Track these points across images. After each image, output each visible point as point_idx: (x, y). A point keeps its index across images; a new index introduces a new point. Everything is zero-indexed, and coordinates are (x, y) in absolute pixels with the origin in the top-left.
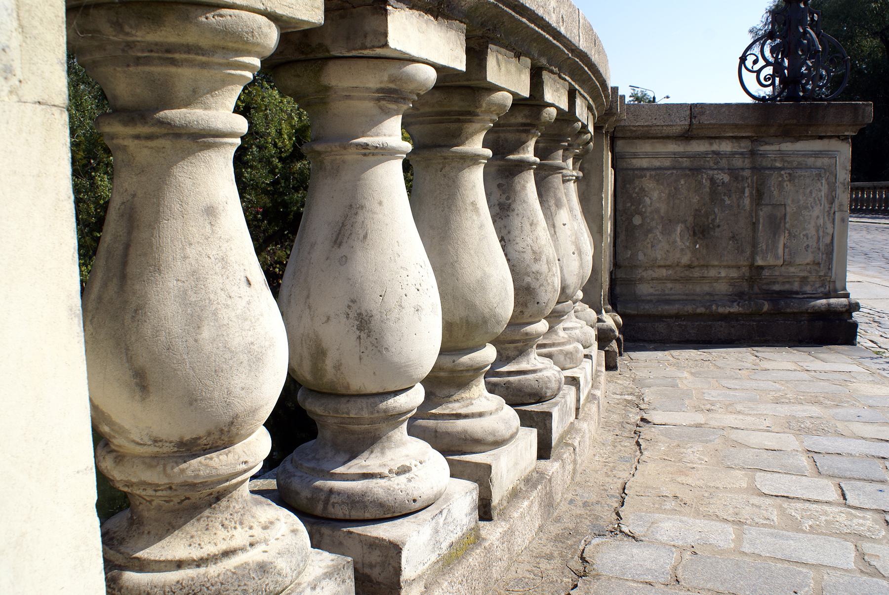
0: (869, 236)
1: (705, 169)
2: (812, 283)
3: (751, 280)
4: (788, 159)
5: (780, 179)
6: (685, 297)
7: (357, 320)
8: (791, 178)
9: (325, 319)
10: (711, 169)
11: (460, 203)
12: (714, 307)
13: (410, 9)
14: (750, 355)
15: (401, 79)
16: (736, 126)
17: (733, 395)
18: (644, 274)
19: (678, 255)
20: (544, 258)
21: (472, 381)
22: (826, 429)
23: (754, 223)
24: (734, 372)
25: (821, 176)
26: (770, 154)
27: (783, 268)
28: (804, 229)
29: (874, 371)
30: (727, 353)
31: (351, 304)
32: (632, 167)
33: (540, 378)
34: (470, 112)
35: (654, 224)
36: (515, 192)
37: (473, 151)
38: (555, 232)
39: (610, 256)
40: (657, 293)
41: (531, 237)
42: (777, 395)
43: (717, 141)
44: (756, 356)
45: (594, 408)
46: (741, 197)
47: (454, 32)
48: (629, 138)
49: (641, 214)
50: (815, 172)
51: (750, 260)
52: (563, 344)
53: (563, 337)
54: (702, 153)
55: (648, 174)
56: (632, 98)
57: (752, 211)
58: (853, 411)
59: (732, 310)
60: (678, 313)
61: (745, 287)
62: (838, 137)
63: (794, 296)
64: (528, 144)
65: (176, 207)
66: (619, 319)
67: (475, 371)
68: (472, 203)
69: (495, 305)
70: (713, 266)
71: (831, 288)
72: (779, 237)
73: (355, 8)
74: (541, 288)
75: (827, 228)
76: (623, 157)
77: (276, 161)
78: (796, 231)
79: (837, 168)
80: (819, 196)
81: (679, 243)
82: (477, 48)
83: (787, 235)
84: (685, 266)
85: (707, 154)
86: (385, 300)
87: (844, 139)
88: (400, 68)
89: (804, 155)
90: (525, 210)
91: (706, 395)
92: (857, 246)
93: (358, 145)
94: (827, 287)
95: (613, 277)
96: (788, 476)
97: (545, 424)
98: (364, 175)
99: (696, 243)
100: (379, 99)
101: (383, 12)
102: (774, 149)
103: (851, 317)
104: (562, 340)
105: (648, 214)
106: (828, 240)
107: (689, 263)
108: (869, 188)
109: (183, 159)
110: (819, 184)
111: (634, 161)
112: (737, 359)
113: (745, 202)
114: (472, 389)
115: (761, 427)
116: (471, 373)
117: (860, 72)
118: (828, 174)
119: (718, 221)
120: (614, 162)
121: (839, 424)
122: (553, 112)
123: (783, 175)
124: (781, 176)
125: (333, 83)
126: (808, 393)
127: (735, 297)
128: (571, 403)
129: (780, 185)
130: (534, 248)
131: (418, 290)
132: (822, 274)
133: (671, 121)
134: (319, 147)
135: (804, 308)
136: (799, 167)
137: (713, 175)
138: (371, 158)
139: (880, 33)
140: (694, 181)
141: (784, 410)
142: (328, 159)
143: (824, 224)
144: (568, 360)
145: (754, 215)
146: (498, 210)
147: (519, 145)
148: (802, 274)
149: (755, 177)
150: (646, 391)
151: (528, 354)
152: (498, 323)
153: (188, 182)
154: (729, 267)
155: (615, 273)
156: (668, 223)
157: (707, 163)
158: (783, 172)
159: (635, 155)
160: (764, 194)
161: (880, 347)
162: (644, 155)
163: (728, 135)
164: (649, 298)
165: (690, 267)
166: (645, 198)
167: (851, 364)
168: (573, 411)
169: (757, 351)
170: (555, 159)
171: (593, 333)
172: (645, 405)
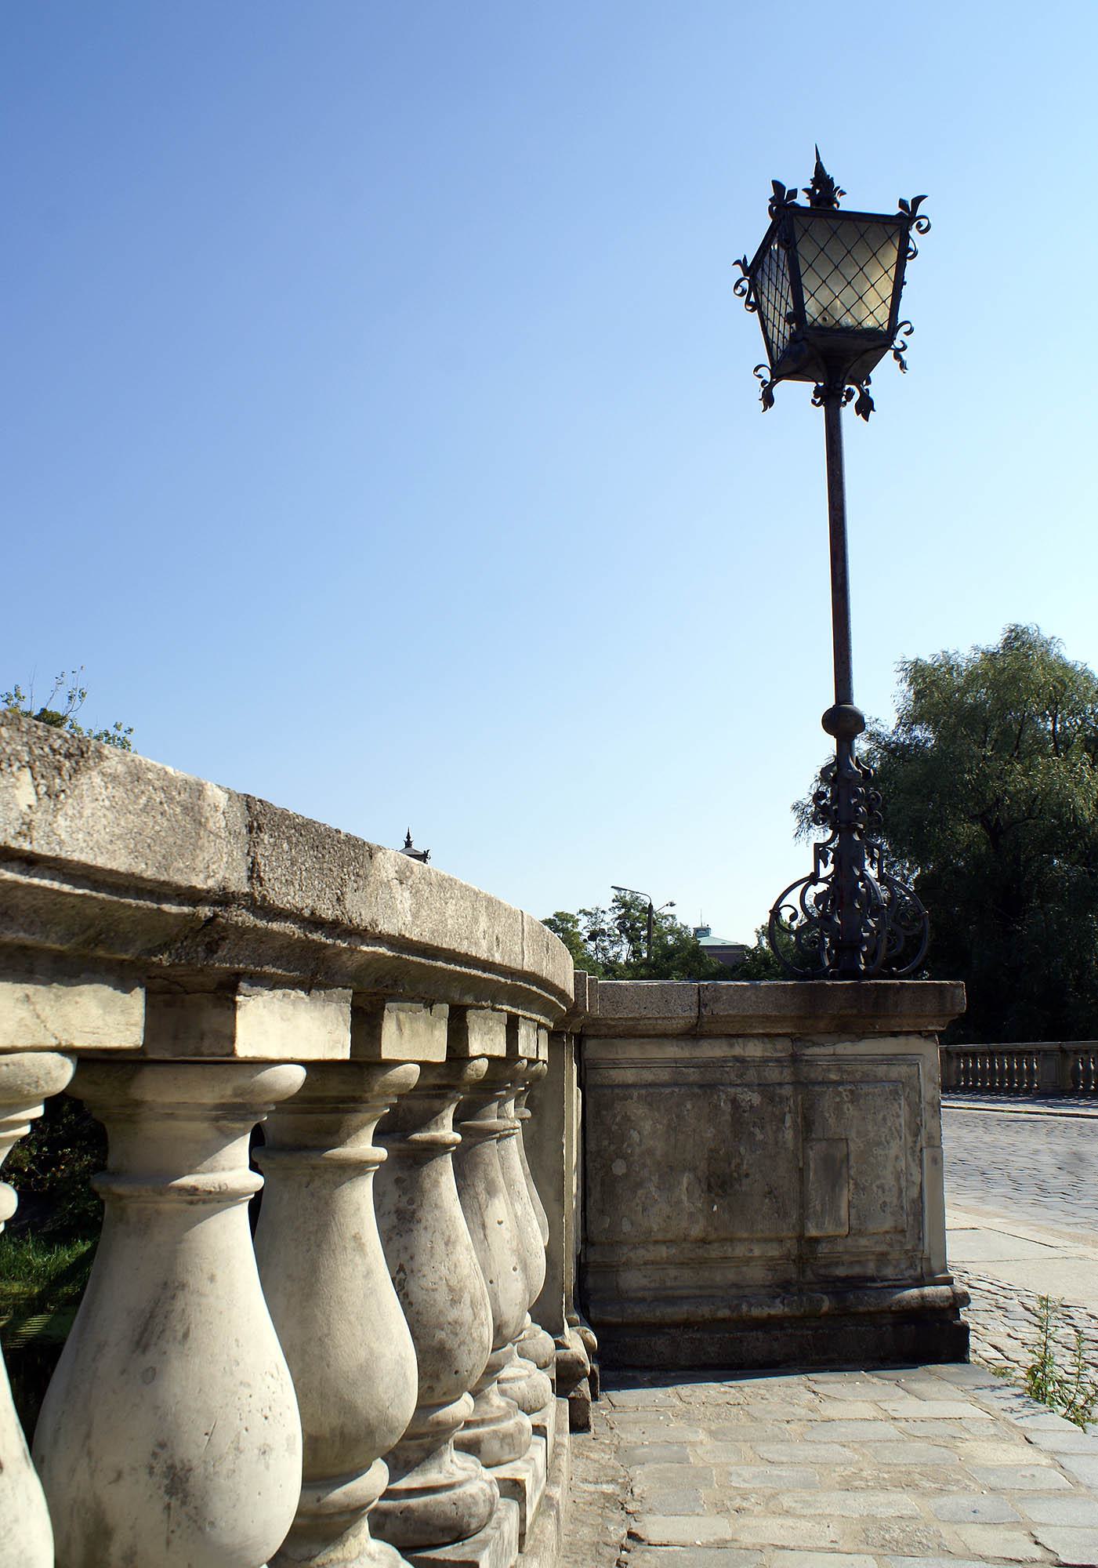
0: (987, 1138)
1: (723, 1085)
2: (894, 1262)
3: (801, 1261)
5: (838, 1099)
6: (698, 1292)
7: (166, 1477)
8: (855, 1098)
9: (113, 1476)
11: (336, 1239)
12: (744, 1308)
13: (271, 990)
14: (805, 1391)
15: (252, 1091)
16: (768, 1018)
17: (778, 1476)
18: (631, 1254)
19: (684, 1224)
20: (467, 1298)
21: (348, 1528)
22: (924, 1541)
23: (801, 1170)
24: (779, 1428)
25: (897, 1093)
26: (820, 1061)
27: (849, 1239)
28: (878, 1177)
29: (996, 1414)
30: (767, 1387)
31: (158, 1450)
32: (610, 1082)
33: (460, 1499)
34: (354, 1097)
35: (645, 1173)
36: (422, 1192)
37: (358, 1157)
38: (485, 1235)
39: (576, 1231)
40: (653, 1285)
41: (446, 1264)
42: (847, 1472)
43: (740, 1040)
44: (814, 1392)
45: (550, 1526)
46: (779, 1129)
47: (334, 1005)
48: (606, 1036)
49: (624, 1157)
50: (889, 1087)
51: (798, 1228)
53: (498, 1407)
54: (718, 1059)
56: (616, 904)
57: (798, 1149)
58: (965, 1501)
59: (773, 1312)
60: (688, 1319)
61: (792, 1272)
62: (920, 1033)
63: (869, 1285)
64: (443, 1114)
66: (593, 1338)
67: (353, 1512)
68: (355, 1237)
69: (387, 1404)
70: (740, 1240)
71: (924, 1270)
72: (841, 1190)
73: (188, 994)
74: (462, 1347)
75: (911, 1175)
78: (866, 1181)
79: (921, 1080)
80: (897, 1125)
82: (368, 1009)
83: (852, 1186)
85: (725, 1061)
87: (928, 1035)
88: (252, 1077)
89: (874, 1062)
90: (437, 1220)
91: (733, 1478)
92: (970, 1158)
93: (182, 1190)
94: (919, 1269)
95: (582, 1261)
98: (189, 1235)
99: (713, 1202)
100: (217, 1119)
101: (232, 1006)
102: (827, 1052)
103: (958, 1317)
104: (497, 1414)
106: (914, 1192)
107: (701, 1235)
108: (983, 1054)
111: (612, 1072)
113: (786, 1136)
114: (348, 1544)
115: (823, 1544)
117: (957, 871)
118: (908, 1090)
119: (745, 1166)
120: (583, 1074)
121: (946, 1531)
122: (483, 1065)
123: (841, 1092)
125: (149, 1096)
126: (895, 1465)
127: (778, 1290)
128: (511, 1532)
129: (838, 1109)
130: (451, 1283)
131: (266, 1418)
132: (909, 1247)
134: (120, 1189)
135: (885, 1304)
136: (866, 1079)
137: (736, 1094)
138: (200, 1207)
139: (981, 816)
141: (858, 1504)
144: (506, 1448)
146: (396, 1221)
147: (429, 1118)
148: (879, 1249)
149: (800, 1097)
150: (638, 1472)
151: (441, 1455)
152: (392, 1431)
154: (766, 1240)
155: (585, 1254)
156: (669, 1171)
157: (726, 1075)
158: (840, 1089)
159: (614, 1063)
160: (814, 1124)
161: (1007, 1358)
163: (755, 1032)
164: (640, 1294)
165: (704, 1241)
167: (963, 1401)
168: (514, 1543)
169: (816, 1382)
170: (485, 1118)
171: (544, 1380)
172: (634, 1503)
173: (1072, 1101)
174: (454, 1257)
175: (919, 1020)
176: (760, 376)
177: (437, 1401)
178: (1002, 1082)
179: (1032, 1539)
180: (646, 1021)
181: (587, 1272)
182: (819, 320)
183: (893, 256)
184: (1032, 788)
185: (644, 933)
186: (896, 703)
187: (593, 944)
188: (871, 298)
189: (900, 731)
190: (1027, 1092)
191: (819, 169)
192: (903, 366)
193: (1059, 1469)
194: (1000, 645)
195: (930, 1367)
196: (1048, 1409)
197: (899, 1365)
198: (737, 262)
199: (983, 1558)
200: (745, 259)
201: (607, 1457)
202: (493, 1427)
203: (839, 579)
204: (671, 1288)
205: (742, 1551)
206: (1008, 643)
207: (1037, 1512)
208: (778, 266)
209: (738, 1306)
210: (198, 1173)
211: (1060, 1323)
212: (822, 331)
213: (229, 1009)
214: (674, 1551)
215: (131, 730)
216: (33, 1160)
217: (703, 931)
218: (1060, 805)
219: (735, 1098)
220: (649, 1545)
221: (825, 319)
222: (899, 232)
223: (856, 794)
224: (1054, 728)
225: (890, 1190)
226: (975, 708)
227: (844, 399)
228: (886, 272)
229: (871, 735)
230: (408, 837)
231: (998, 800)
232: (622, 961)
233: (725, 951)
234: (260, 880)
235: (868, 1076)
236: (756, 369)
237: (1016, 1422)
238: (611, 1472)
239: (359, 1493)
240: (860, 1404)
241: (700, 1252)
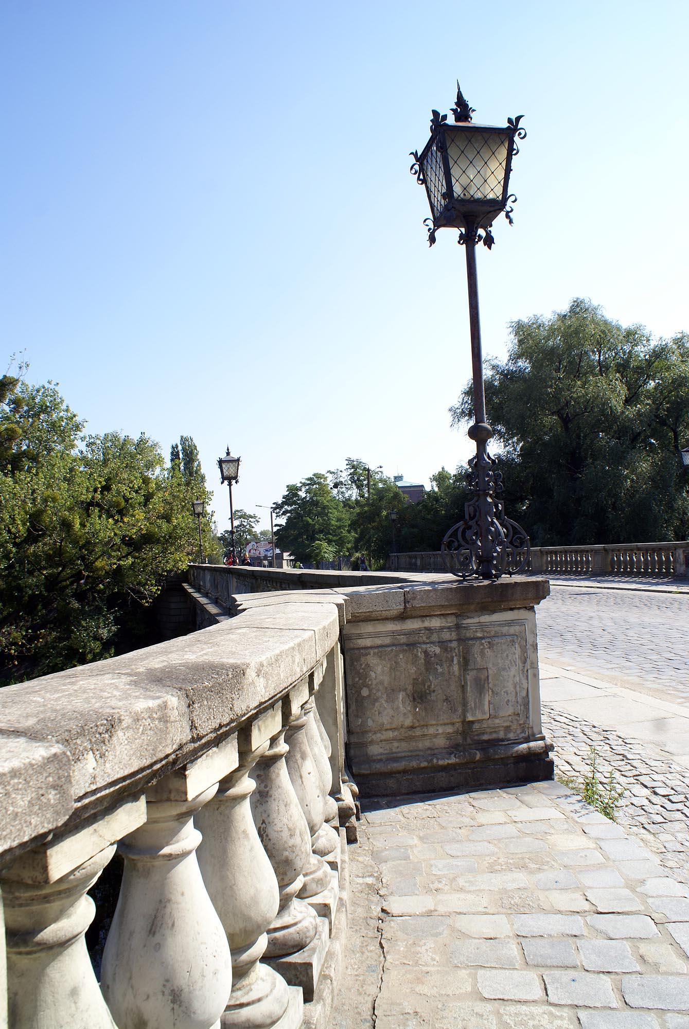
0: (564, 609)
1: (419, 644)
2: (514, 731)
4: (487, 630)
5: (482, 647)
6: (409, 754)
8: (491, 645)
9: (146, 997)
10: (425, 643)
11: (234, 835)
12: (435, 761)
18: (374, 737)
19: (401, 719)
22: (531, 904)
23: (463, 686)
24: (456, 833)
25: (514, 641)
27: (489, 720)
28: (504, 687)
31: (165, 983)
35: (379, 694)
36: (271, 781)
40: (386, 752)
43: (428, 618)
45: (343, 917)
46: (450, 665)
49: (368, 686)
51: (462, 717)
52: (314, 872)
53: (314, 864)
54: (416, 630)
55: (372, 652)
56: (348, 466)
59: (450, 762)
60: (405, 769)
61: (460, 740)
62: (526, 608)
65: (50, 999)
68: (243, 831)
72: (485, 695)
76: (350, 639)
77: (10, 546)
81: (402, 708)
83: (490, 693)
84: (408, 728)
86: (192, 974)
90: (280, 794)
91: (433, 868)
93: (164, 856)
96: (503, 971)
97: (307, 973)
98: (170, 875)
99: (416, 707)
105: (374, 686)
106: (524, 694)
107: (411, 724)
108: (561, 552)
109: (54, 960)
110: (513, 648)
111: (359, 641)
112: (457, 813)
113: (454, 669)
115: (481, 909)
116: (249, 965)
119: (433, 686)
124: (482, 644)
129: (482, 653)
132: (521, 722)
133: (389, 606)
135: (509, 754)
138: (174, 861)
140: (411, 655)
141: (497, 881)
142: (140, 865)
143: (520, 681)
144: (319, 886)
145: (462, 678)
148: (506, 724)
149: (461, 647)
151: (289, 907)
153: (58, 976)
156: (392, 692)
157: (421, 638)
158: (483, 641)
159: (360, 636)
162: (367, 635)
164: (379, 757)
165: (412, 727)
166: (371, 672)
167: (550, 807)
169: (474, 798)
173: (611, 578)
174: (290, 812)
175: (525, 602)
176: (427, 225)
177: (286, 883)
178: (571, 568)
179: (585, 897)
180: (376, 613)
181: (350, 748)
182: (462, 196)
183: (503, 153)
184: (587, 395)
185: (365, 482)
186: (507, 347)
187: (336, 490)
188: (492, 182)
189: (510, 364)
190: (586, 573)
191: (460, 96)
192: (511, 222)
193: (599, 850)
194: (568, 310)
195: (534, 784)
196: (595, 809)
197: (517, 784)
198: (412, 153)
199: (560, 912)
200: (416, 152)
201: (367, 859)
202: (312, 876)
203: (476, 345)
204: (396, 753)
205: (440, 917)
206: (573, 310)
207: (588, 880)
208: (436, 161)
209: (432, 760)
210: (171, 844)
211: (602, 743)
212: (463, 201)
213: (183, 778)
214: (406, 919)
215: (58, 384)
216: (24, 637)
217: (399, 478)
218: (603, 404)
219: (426, 651)
220: (393, 916)
221: (465, 195)
222: (507, 139)
223: (488, 475)
224: (599, 359)
225: (511, 693)
226: (553, 349)
227: (476, 240)
228: (501, 164)
229: (493, 367)
230: (228, 450)
231: (567, 402)
232: (354, 498)
233: (412, 489)
234: (196, 727)
235: (498, 633)
236: (425, 221)
237: (577, 819)
238: (370, 869)
239: (255, 954)
240: (497, 813)
241: (410, 733)
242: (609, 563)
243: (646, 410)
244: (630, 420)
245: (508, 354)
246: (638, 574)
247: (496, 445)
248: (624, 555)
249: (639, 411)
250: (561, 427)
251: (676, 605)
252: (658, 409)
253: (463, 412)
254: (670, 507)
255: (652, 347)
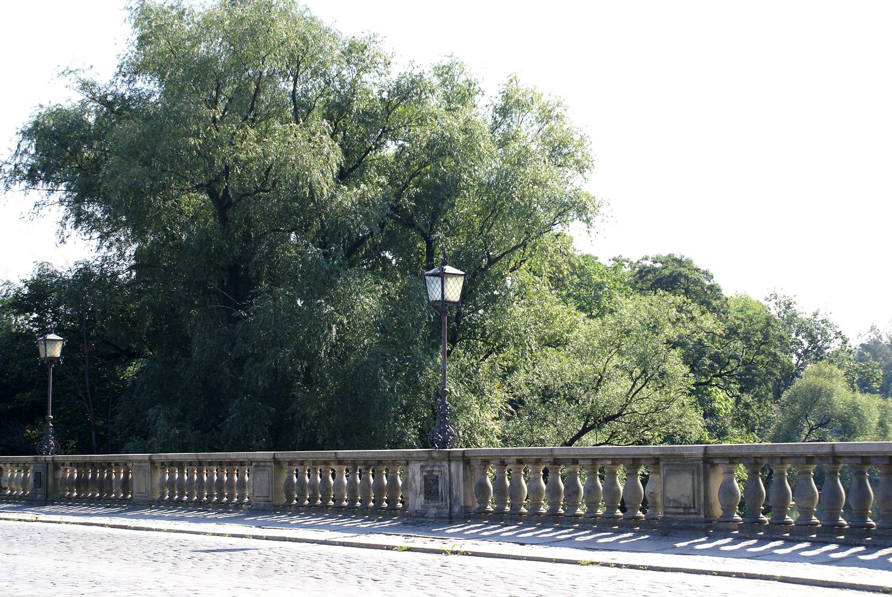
173: (284, 518)
178: (210, 496)
189: (119, 82)
190: (238, 507)
224: (294, 91)
226: (206, 64)
231: (227, 168)
242: (282, 488)
243: (376, 195)
244: (345, 212)
245: (119, 62)
246: (339, 511)
247: (81, 244)
248: (351, 473)
249: (363, 195)
250: (214, 215)
251: (395, 575)
252: (399, 195)
253: (17, 171)
254: (413, 385)
255: (394, 77)
